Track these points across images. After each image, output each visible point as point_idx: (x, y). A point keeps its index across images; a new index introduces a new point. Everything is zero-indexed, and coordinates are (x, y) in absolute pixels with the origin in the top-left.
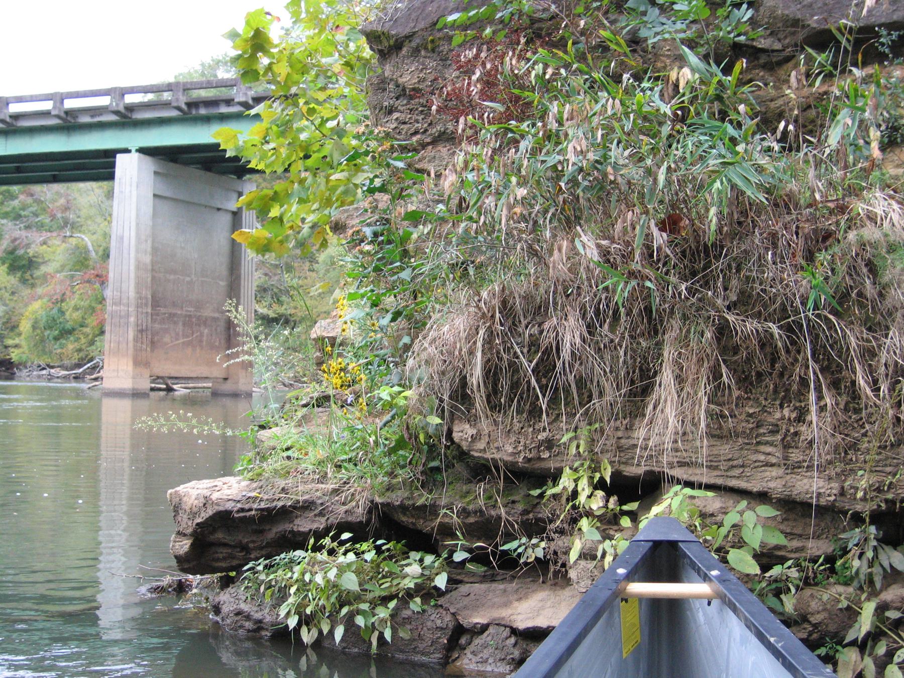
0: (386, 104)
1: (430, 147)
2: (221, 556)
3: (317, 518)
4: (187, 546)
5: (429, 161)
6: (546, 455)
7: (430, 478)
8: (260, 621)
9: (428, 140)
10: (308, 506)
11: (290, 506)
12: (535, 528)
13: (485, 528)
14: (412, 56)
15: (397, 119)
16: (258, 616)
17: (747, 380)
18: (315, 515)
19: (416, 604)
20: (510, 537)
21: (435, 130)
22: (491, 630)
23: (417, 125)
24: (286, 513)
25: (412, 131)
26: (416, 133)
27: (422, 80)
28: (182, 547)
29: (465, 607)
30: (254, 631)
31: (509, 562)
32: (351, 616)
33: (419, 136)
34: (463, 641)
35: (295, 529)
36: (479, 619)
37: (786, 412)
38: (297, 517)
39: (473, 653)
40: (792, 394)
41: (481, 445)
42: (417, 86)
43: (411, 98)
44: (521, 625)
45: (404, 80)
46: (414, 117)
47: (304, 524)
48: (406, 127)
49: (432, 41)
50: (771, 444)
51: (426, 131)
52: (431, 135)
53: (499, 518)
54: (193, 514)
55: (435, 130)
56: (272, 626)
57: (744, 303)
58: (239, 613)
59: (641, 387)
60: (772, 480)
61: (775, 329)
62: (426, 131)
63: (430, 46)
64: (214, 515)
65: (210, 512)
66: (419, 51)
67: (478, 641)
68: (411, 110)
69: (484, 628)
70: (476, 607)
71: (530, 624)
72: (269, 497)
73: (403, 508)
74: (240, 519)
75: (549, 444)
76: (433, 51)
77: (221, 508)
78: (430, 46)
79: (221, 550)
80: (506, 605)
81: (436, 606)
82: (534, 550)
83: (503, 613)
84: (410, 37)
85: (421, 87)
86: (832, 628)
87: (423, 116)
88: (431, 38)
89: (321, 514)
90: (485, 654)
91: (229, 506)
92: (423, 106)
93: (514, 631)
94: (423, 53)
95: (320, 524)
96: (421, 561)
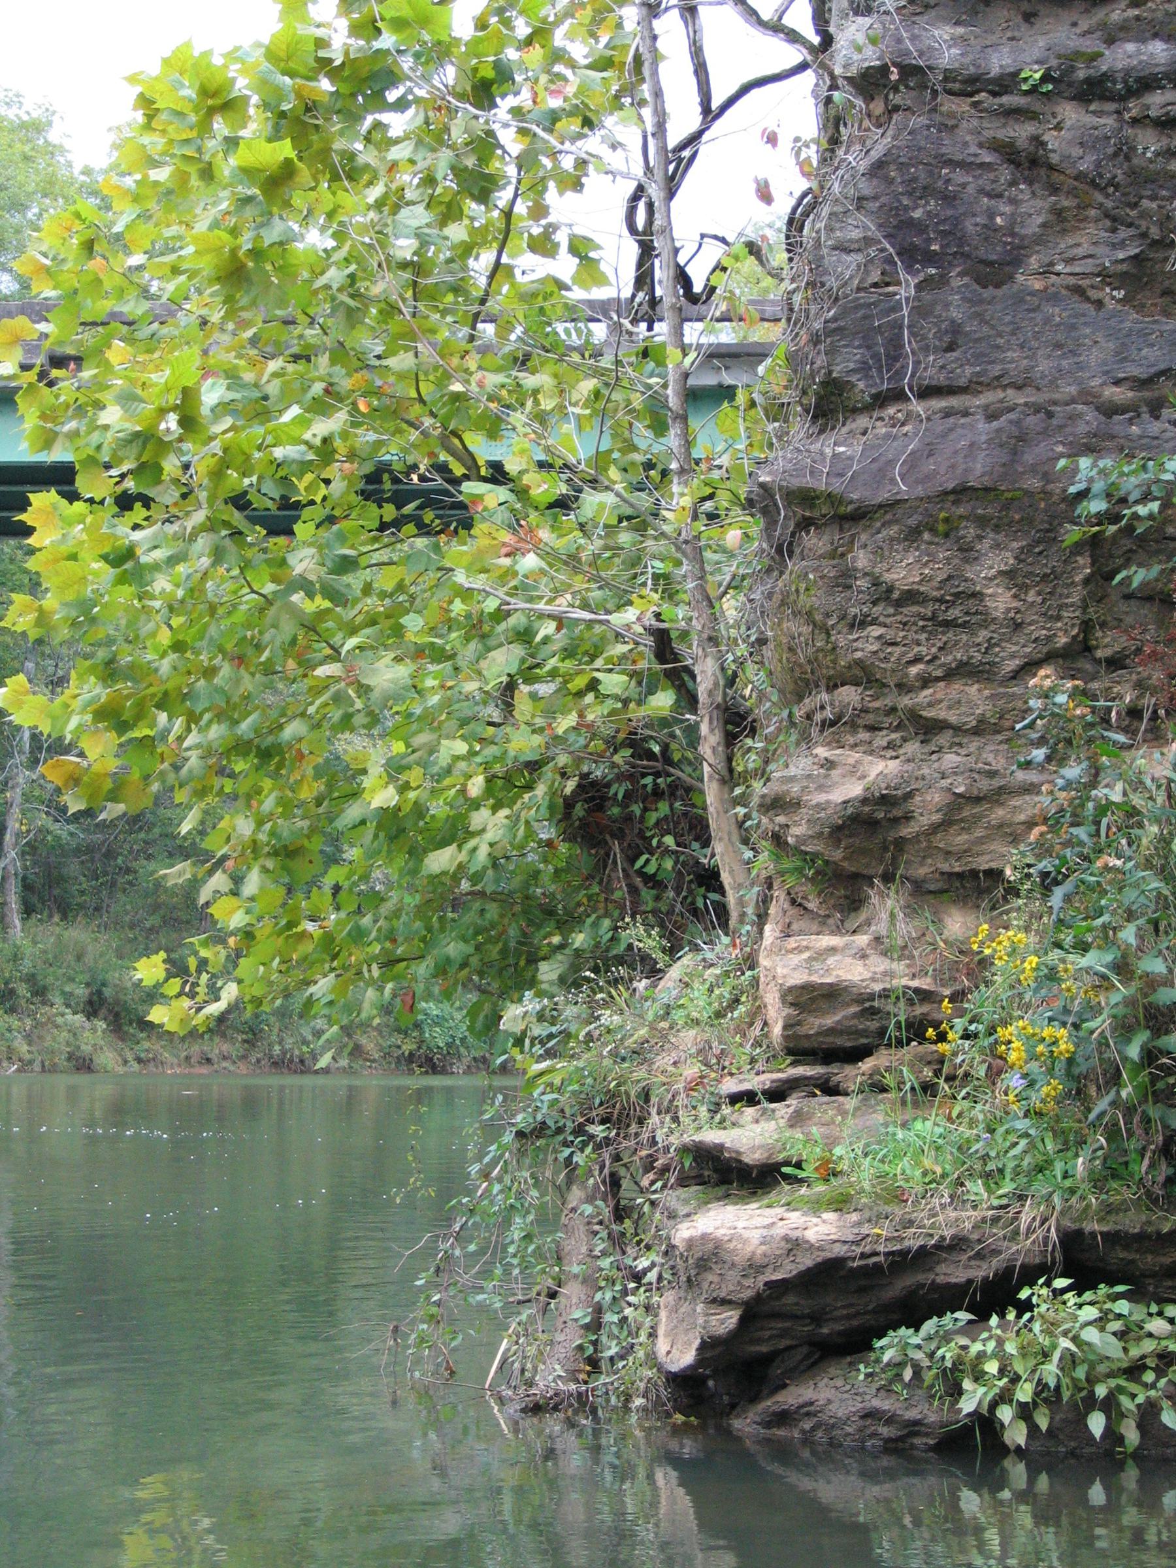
0: (853, 611)
1: (942, 684)
2: (768, 1333)
3: (973, 1263)
4: (735, 1320)
5: (950, 708)
8: (917, 1423)
9: (939, 673)
10: (958, 1244)
11: (934, 1246)
14: (905, 539)
15: (880, 637)
16: (912, 1414)
18: (970, 1258)
21: (950, 658)
23: (917, 649)
24: (924, 1257)
25: (910, 656)
26: (917, 660)
27: (924, 580)
28: (722, 1322)
33: (921, 666)
35: (940, 1279)
38: (938, 1263)
42: (916, 587)
43: (898, 604)
45: (896, 576)
46: (912, 635)
48: (897, 650)
49: (946, 520)
51: (935, 658)
52: (943, 665)
54: (754, 1267)
55: (950, 658)
56: (942, 1427)
58: (871, 1415)
62: (935, 658)
63: (941, 528)
64: (818, 1265)
65: (807, 1261)
66: (920, 533)
68: (905, 624)
72: (882, 1236)
76: (946, 535)
77: (829, 1255)
78: (941, 528)
79: (773, 1325)
85: (922, 589)
87: (925, 635)
88: (943, 515)
89: (979, 1256)
91: (839, 1250)
92: (924, 619)
94: (926, 536)
95: (983, 1271)
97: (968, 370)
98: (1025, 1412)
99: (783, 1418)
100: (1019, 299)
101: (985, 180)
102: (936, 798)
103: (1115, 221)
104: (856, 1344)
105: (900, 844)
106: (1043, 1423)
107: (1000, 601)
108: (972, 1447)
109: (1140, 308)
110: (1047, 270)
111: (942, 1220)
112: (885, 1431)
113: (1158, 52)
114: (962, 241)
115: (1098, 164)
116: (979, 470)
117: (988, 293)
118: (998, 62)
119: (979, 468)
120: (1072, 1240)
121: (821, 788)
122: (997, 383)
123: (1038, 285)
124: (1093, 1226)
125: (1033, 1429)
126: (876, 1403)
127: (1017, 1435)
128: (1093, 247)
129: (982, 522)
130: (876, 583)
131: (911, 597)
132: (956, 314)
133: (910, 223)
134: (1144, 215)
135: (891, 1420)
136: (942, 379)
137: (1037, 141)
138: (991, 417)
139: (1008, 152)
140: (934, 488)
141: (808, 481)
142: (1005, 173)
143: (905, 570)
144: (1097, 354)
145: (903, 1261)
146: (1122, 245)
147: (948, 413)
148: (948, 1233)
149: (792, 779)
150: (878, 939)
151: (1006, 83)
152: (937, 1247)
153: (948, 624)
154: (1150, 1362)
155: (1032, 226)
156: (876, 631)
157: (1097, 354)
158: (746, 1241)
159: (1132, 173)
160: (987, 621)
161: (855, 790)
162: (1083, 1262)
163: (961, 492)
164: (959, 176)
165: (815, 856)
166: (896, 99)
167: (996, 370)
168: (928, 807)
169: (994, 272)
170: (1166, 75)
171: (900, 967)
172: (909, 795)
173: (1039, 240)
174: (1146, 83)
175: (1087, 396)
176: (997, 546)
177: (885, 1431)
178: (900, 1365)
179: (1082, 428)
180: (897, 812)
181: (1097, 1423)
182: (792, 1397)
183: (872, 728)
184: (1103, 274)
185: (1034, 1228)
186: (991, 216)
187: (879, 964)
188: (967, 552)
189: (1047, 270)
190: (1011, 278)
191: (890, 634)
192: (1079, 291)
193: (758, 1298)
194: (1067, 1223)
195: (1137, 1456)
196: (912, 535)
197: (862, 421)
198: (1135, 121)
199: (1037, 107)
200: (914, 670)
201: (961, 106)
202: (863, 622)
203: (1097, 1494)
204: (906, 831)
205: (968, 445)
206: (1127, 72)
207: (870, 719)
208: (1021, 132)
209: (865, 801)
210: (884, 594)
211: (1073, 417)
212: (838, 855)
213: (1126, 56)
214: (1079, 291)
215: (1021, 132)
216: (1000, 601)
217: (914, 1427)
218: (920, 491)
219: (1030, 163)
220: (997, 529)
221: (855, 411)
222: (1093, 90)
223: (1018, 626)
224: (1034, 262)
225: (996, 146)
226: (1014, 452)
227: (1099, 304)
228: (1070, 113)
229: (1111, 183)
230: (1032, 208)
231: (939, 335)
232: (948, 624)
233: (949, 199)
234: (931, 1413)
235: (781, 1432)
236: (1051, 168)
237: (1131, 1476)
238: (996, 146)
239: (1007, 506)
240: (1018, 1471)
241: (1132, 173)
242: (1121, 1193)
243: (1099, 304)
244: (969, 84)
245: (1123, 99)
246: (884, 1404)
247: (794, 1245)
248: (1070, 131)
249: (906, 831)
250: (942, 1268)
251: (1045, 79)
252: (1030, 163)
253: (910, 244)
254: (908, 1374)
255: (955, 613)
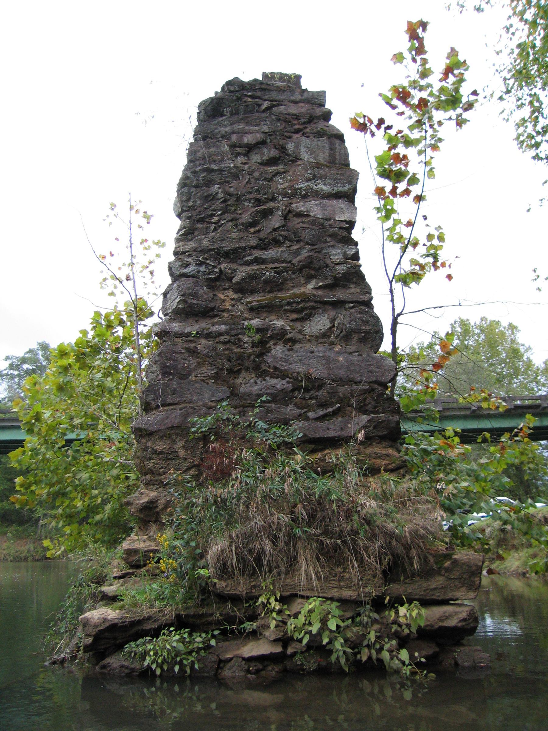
6: (254, 591)
7: (203, 603)
8: (133, 669)
10: (149, 618)
12: (253, 618)
13: (230, 619)
16: (132, 666)
17: (329, 558)
19: (202, 653)
20: (241, 623)
22: (234, 659)
24: (139, 622)
26: (162, 468)
29: (222, 652)
30: (130, 673)
31: (241, 632)
32: (181, 661)
34: (222, 665)
36: (229, 656)
37: (340, 569)
39: (229, 669)
40: (342, 562)
41: (228, 589)
43: (159, 454)
44: (246, 655)
47: (148, 626)
50: (334, 580)
53: (236, 616)
54: (96, 626)
57: (326, 533)
58: (122, 666)
59: (292, 562)
60: (335, 593)
61: (339, 542)
65: (107, 624)
67: (230, 664)
69: (231, 659)
70: (226, 651)
71: (250, 655)
72: (129, 616)
73: (194, 616)
74: (122, 626)
75: (255, 586)
80: (239, 649)
81: (209, 653)
82: (249, 626)
83: (239, 652)
84: (157, 431)
86: (358, 642)
89: (155, 621)
90: (234, 669)
91: (116, 621)
93: (244, 659)
95: (155, 625)
96: (200, 636)
97: (178, 399)
98: (160, 666)
99: (104, 667)
100: (189, 383)
101: (183, 356)
102: (163, 501)
103: (211, 365)
104: (120, 647)
105: (158, 513)
106: (165, 668)
107: (182, 453)
108: (147, 675)
109: (217, 384)
110: (196, 376)
111: (146, 612)
112: (126, 671)
113: (223, 327)
114: (177, 370)
115: (208, 352)
116: (177, 422)
117: (182, 381)
118: (187, 330)
119: (177, 421)
120: (178, 616)
121: (138, 499)
122: (185, 402)
123: (194, 379)
124: (182, 613)
125: (162, 670)
126: (124, 663)
127: (158, 672)
128: (207, 370)
129: (177, 434)
130: (153, 450)
131: (161, 453)
132: (174, 386)
133: (167, 366)
134: (218, 363)
135: (127, 668)
136: (172, 402)
137: (195, 347)
138: (181, 409)
139: (188, 350)
140: (166, 426)
141: (140, 426)
142: (187, 354)
143: (159, 446)
144: (207, 396)
145: (133, 624)
146: (213, 370)
147: (172, 409)
148: (146, 615)
149: (132, 497)
150: (150, 537)
151: (189, 335)
152: (143, 619)
153: (170, 459)
154: (196, 650)
155: (193, 366)
156: (153, 461)
157: (207, 396)
158: (94, 619)
159: (217, 354)
160: (179, 458)
161: (146, 500)
162: (180, 623)
163: (173, 427)
164: (177, 355)
165: (137, 516)
166: (165, 339)
167: (184, 399)
168: (161, 504)
169: (184, 377)
170: (225, 332)
171: (153, 544)
172: (157, 501)
173: (195, 369)
174: (220, 334)
175: (205, 405)
176: (180, 440)
177: (126, 671)
178: (131, 653)
179: (202, 412)
180: (155, 505)
181: (177, 668)
182: (105, 662)
183: (154, 485)
184: (208, 376)
185: (169, 613)
186: (184, 364)
187: (148, 543)
188: (174, 441)
189: (196, 376)
190: (188, 378)
191: (156, 462)
192: (203, 381)
193: (97, 634)
194: (177, 612)
195: (190, 676)
196: (161, 438)
197: (154, 412)
198: (217, 343)
199: (195, 340)
200: (161, 470)
201: (179, 340)
202: (150, 459)
203: (176, 688)
204: (158, 510)
205: (174, 416)
206: (216, 332)
207: (153, 482)
208: (191, 346)
209: (147, 502)
210: (155, 452)
211: (200, 410)
212: (142, 516)
213: (216, 328)
214: (203, 381)
215: (191, 346)
216: (182, 453)
217: (133, 670)
218: (163, 427)
219: (193, 352)
220: (181, 436)
221: (153, 410)
222: (208, 336)
223: (186, 459)
224: (193, 374)
225: (185, 348)
226: (185, 418)
227: (208, 383)
228: (203, 341)
229: (211, 356)
230: (193, 362)
231: (171, 391)
232: (170, 459)
233: (175, 360)
234: (136, 665)
235: (104, 671)
236: (198, 353)
237: (188, 682)
238: (185, 348)
239: (183, 430)
240: (158, 682)
241: (217, 354)
242: (191, 603)
243: (208, 383)
244: (180, 335)
245: (215, 338)
246: (125, 663)
247: (105, 620)
248: (203, 345)
249: (158, 510)
250: (145, 625)
251: (197, 333)
252: (193, 352)
253: (165, 373)
254: (133, 655)
255: (171, 456)
